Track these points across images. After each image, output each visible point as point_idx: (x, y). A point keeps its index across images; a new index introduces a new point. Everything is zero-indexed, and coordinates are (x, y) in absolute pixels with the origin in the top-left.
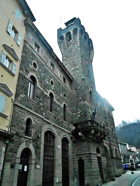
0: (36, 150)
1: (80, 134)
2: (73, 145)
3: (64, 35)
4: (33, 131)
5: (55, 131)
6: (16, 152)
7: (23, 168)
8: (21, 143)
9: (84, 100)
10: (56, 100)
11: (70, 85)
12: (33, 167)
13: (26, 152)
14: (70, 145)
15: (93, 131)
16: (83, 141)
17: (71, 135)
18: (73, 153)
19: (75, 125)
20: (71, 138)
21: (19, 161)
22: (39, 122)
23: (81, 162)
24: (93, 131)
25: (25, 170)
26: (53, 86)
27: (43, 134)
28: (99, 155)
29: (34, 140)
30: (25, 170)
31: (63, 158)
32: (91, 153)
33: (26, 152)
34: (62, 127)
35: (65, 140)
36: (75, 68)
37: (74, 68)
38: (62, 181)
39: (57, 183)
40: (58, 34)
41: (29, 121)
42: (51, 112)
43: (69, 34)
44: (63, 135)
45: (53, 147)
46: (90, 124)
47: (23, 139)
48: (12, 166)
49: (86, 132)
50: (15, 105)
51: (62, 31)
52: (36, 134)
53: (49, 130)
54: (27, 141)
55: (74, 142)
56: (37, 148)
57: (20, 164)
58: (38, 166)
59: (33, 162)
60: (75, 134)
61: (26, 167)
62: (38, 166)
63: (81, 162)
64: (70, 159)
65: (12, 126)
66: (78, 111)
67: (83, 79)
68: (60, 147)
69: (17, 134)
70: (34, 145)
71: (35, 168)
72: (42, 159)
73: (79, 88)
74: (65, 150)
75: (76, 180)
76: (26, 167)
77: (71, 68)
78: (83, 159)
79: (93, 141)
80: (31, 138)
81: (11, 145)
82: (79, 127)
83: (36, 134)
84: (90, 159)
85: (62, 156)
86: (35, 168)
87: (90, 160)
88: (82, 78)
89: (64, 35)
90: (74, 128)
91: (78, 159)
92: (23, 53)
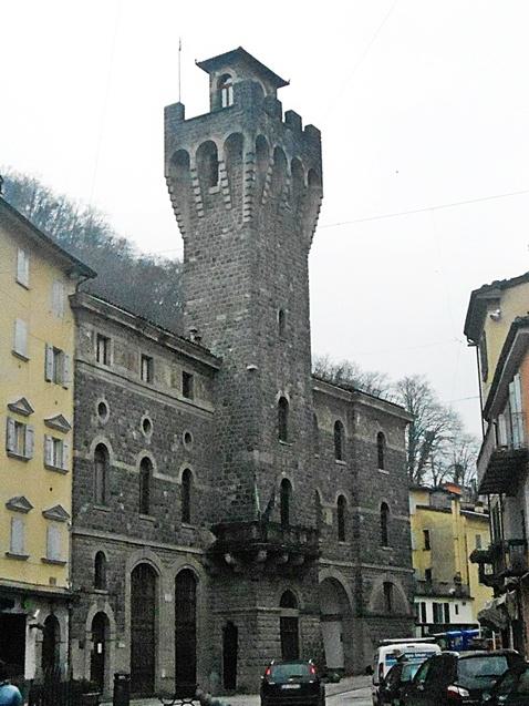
0: (116, 615)
1: (228, 558)
2: (210, 585)
3: (192, 151)
4: (108, 576)
5: (156, 560)
6: (85, 622)
7: (96, 647)
8: (90, 604)
9: (250, 449)
10: (161, 472)
11: (209, 388)
12: (112, 645)
13: (100, 620)
14: (200, 587)
15: (263, 555)
16: (240, 576)
17: (204, 559)
18: (212, 608)
19: (216, 530)
20: (206, 567)
21: (89, 636)
22: (118, 552)
23: (231, 633)
24: (263, 555)
25: (100, 651)
26: (151, 435)
27: (128, 575)
28: (291, 612)
29: (113, 595)
30: (100, 651)
31: (177, 623)
32: (258, 610)
33: (100, 620)
34: (176, 543)
35: (185, 579)
36: (228, 317)
37: (224, 317)
38: (173, 675)
39: (163, 679)
40: (165, 133)
41: (100, 556)
42: (146, 513)
43: (208, 149)
44: (179, 564)
45: (153, 601)
46: (255, 532)
47: (93, 596)
48: (81, 647)
49: (246, 555)
50: (74, 536)
51: (185, 126)
52: (115, 580)
53: (146, 562)
54: (98, 601)
55: (213, 576)
56: (117, 608)
57: (92, 640)
58: (122, 645)
59: (113, 637)
60: (214, 555)
61: (100, 645)
62: (122, 645)
63: (231, 633)
64: (200, 624)
65: (71, 579)
66: (231, 484)
67: (250, 370)
68: (169, 597)
69: (82, 590)
70: (111, 605)
71: (117, 646)
72: (128, 631)
73: (237, 399)
74: (184, 603)
75: (214, 676)
76: (100, 645)
77: (217, 313)
78: (236, 624)
79: (272, 577)
80: (106, 592)
81: (76, 611)
82: (228, 538)
83: (115, 580)
84: (255, 626)
85: (177, 668)
86: (117, 646)
87: (254, 629)
88: (249, 367)
89: (192, 151)
90: (214, 539)
91: (224, 624)
92: (75, 398)
